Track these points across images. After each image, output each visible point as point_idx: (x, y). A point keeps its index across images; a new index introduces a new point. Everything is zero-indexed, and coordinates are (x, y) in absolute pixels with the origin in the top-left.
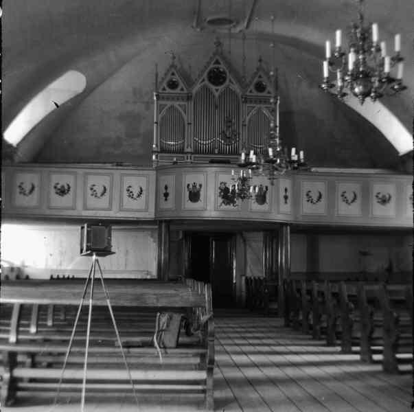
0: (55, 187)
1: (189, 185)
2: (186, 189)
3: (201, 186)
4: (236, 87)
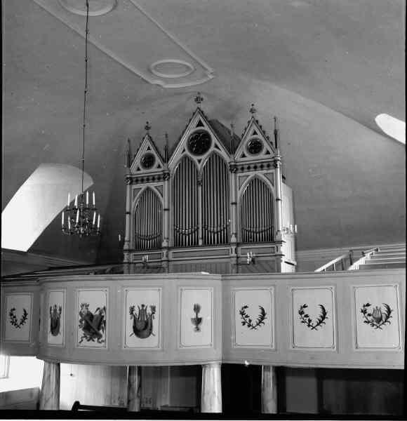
2: (129, 315)
3: (153, 309)
4: (223, 153)
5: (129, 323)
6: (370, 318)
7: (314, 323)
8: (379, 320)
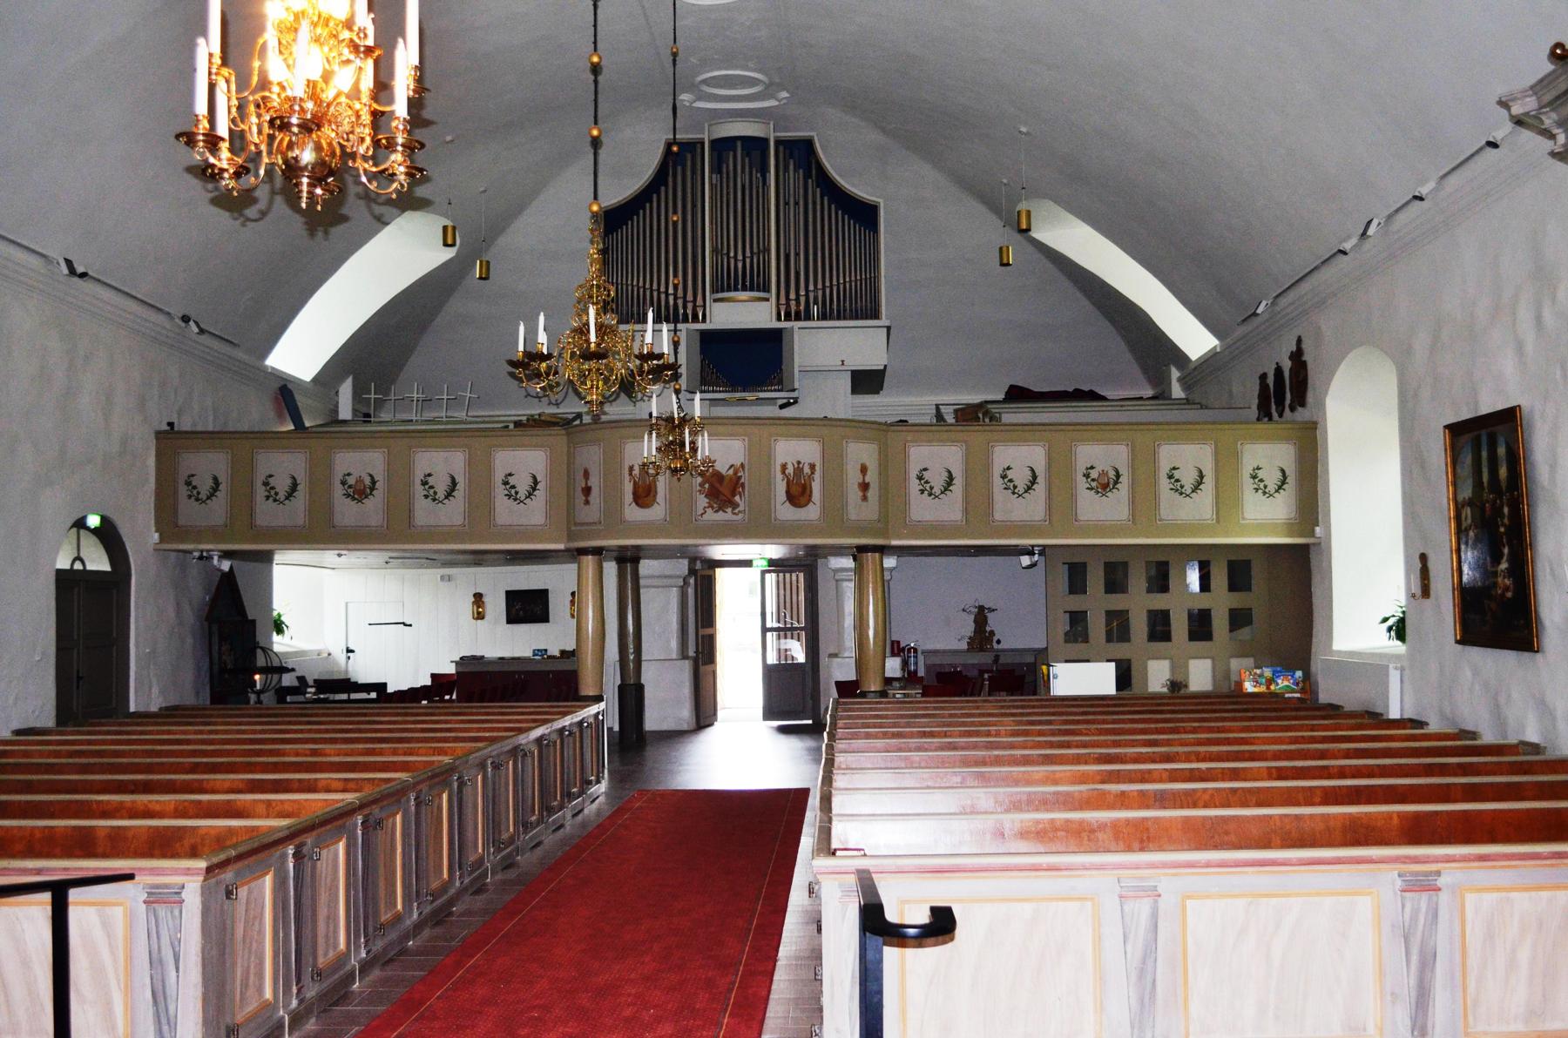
0: (343, 483)
1: (631, 469)
2: (779, 476)
3: (812, 467)
5: (628, 488)
6: (351, 491)
7: (1020, 489)
8: (1105, 487)
